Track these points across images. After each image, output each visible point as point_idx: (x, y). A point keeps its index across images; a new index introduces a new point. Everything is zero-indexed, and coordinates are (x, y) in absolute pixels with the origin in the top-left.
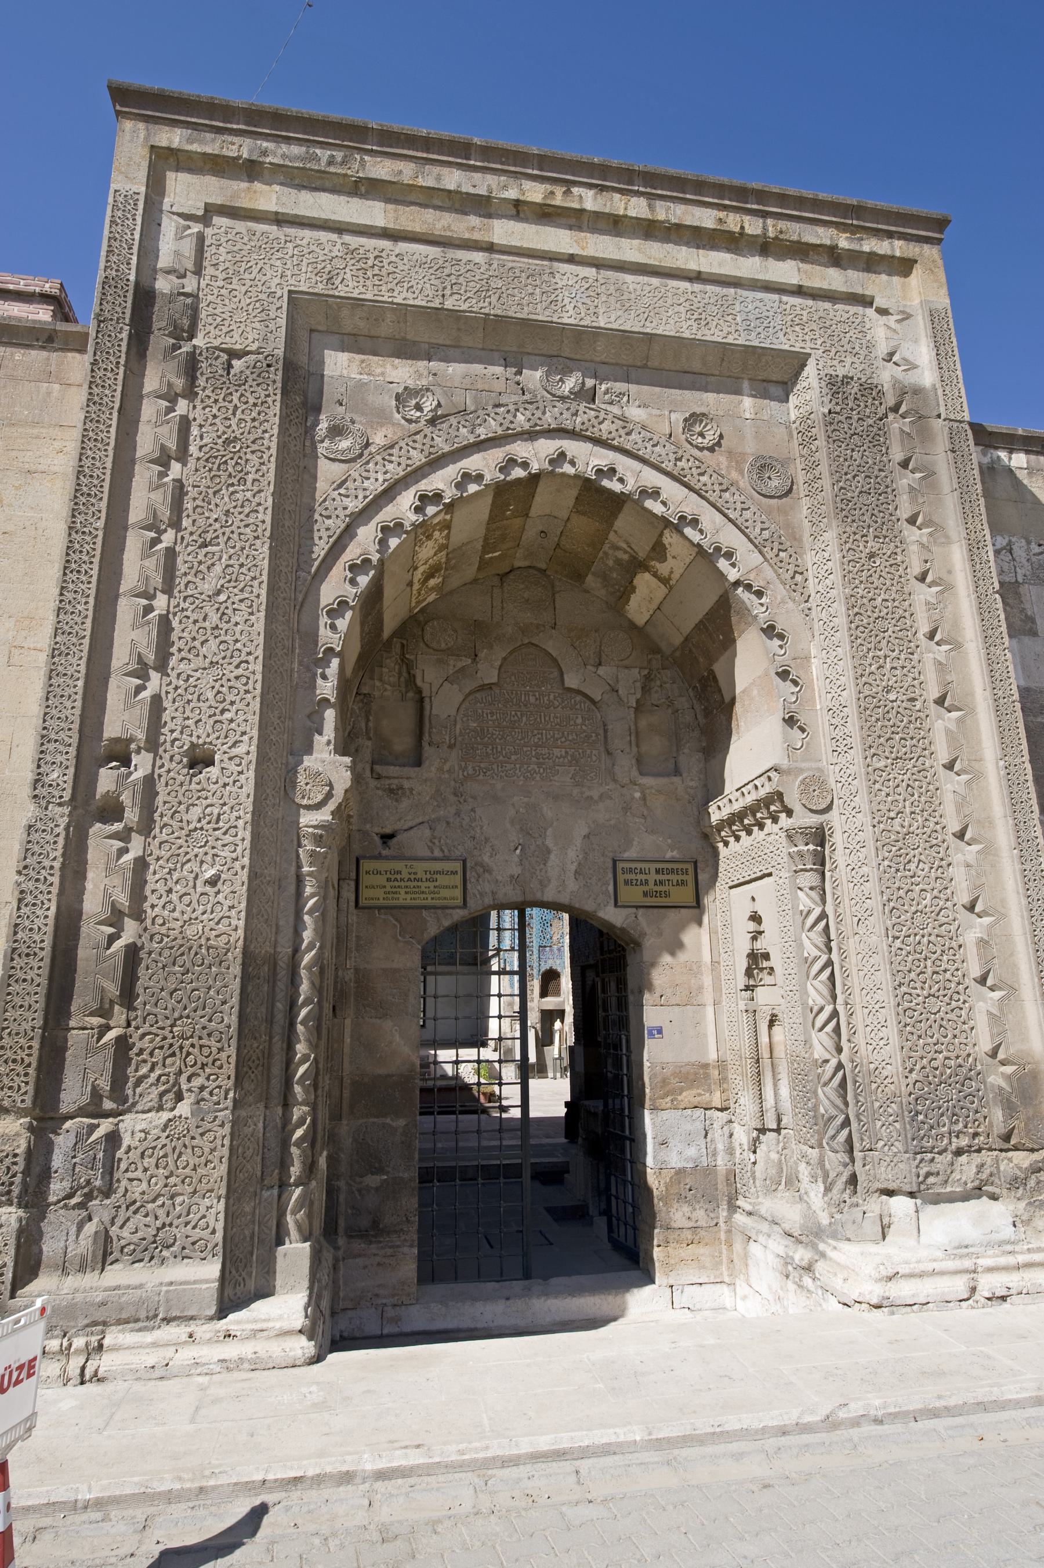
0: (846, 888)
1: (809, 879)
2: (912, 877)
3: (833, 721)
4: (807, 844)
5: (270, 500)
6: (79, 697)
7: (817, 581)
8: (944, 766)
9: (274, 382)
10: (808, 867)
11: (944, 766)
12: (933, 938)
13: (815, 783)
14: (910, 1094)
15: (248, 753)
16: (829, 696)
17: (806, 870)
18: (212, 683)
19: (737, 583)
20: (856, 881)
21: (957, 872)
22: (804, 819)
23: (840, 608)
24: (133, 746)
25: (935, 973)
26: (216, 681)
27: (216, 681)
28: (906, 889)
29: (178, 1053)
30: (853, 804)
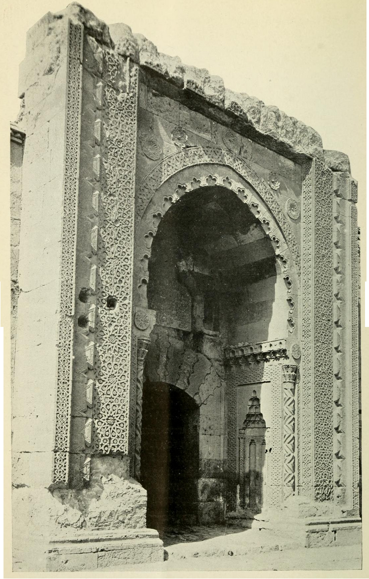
0: (301, 390)
1: (290, 386)
2: (110, 398)
3: (304, 324)
4: (292, 372)
5: (134, 177)
6: (74, 264)
7: (304, 262)
8: (335, 348)
9: (134, 113)
10: (291, 381)
11: (335, 348)
12: (326, 413)
13: (297, 349)
14: (315, 466)
15: (129, 303)
16: (304, 313)
17: (290, 382)
18: (115, 266)
19: (278, 256)
20: (305, 388)
21: (334, 389)
22: (290, 362)
23: (312, 276)
24: (90, 292)
25: (325, 425)
26: (117, 265)
27: (117, 265)
28: (106, 404)
29: (109, 431)
30: (308, 359)
